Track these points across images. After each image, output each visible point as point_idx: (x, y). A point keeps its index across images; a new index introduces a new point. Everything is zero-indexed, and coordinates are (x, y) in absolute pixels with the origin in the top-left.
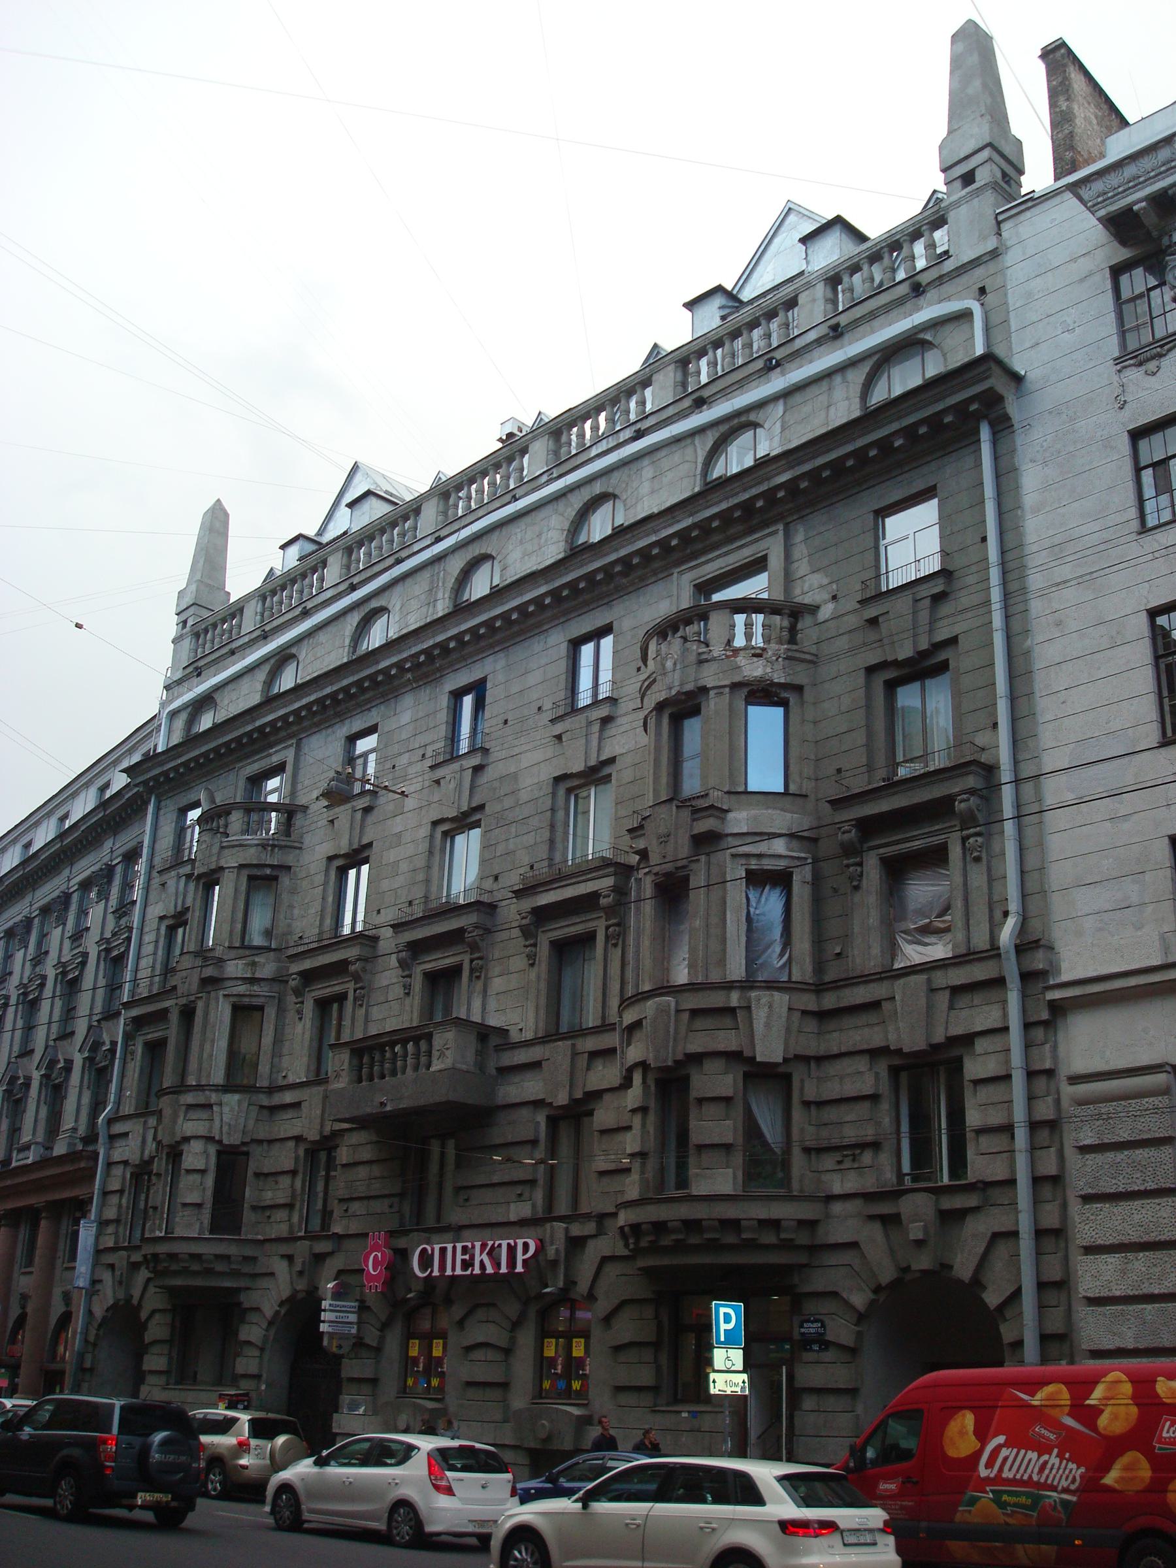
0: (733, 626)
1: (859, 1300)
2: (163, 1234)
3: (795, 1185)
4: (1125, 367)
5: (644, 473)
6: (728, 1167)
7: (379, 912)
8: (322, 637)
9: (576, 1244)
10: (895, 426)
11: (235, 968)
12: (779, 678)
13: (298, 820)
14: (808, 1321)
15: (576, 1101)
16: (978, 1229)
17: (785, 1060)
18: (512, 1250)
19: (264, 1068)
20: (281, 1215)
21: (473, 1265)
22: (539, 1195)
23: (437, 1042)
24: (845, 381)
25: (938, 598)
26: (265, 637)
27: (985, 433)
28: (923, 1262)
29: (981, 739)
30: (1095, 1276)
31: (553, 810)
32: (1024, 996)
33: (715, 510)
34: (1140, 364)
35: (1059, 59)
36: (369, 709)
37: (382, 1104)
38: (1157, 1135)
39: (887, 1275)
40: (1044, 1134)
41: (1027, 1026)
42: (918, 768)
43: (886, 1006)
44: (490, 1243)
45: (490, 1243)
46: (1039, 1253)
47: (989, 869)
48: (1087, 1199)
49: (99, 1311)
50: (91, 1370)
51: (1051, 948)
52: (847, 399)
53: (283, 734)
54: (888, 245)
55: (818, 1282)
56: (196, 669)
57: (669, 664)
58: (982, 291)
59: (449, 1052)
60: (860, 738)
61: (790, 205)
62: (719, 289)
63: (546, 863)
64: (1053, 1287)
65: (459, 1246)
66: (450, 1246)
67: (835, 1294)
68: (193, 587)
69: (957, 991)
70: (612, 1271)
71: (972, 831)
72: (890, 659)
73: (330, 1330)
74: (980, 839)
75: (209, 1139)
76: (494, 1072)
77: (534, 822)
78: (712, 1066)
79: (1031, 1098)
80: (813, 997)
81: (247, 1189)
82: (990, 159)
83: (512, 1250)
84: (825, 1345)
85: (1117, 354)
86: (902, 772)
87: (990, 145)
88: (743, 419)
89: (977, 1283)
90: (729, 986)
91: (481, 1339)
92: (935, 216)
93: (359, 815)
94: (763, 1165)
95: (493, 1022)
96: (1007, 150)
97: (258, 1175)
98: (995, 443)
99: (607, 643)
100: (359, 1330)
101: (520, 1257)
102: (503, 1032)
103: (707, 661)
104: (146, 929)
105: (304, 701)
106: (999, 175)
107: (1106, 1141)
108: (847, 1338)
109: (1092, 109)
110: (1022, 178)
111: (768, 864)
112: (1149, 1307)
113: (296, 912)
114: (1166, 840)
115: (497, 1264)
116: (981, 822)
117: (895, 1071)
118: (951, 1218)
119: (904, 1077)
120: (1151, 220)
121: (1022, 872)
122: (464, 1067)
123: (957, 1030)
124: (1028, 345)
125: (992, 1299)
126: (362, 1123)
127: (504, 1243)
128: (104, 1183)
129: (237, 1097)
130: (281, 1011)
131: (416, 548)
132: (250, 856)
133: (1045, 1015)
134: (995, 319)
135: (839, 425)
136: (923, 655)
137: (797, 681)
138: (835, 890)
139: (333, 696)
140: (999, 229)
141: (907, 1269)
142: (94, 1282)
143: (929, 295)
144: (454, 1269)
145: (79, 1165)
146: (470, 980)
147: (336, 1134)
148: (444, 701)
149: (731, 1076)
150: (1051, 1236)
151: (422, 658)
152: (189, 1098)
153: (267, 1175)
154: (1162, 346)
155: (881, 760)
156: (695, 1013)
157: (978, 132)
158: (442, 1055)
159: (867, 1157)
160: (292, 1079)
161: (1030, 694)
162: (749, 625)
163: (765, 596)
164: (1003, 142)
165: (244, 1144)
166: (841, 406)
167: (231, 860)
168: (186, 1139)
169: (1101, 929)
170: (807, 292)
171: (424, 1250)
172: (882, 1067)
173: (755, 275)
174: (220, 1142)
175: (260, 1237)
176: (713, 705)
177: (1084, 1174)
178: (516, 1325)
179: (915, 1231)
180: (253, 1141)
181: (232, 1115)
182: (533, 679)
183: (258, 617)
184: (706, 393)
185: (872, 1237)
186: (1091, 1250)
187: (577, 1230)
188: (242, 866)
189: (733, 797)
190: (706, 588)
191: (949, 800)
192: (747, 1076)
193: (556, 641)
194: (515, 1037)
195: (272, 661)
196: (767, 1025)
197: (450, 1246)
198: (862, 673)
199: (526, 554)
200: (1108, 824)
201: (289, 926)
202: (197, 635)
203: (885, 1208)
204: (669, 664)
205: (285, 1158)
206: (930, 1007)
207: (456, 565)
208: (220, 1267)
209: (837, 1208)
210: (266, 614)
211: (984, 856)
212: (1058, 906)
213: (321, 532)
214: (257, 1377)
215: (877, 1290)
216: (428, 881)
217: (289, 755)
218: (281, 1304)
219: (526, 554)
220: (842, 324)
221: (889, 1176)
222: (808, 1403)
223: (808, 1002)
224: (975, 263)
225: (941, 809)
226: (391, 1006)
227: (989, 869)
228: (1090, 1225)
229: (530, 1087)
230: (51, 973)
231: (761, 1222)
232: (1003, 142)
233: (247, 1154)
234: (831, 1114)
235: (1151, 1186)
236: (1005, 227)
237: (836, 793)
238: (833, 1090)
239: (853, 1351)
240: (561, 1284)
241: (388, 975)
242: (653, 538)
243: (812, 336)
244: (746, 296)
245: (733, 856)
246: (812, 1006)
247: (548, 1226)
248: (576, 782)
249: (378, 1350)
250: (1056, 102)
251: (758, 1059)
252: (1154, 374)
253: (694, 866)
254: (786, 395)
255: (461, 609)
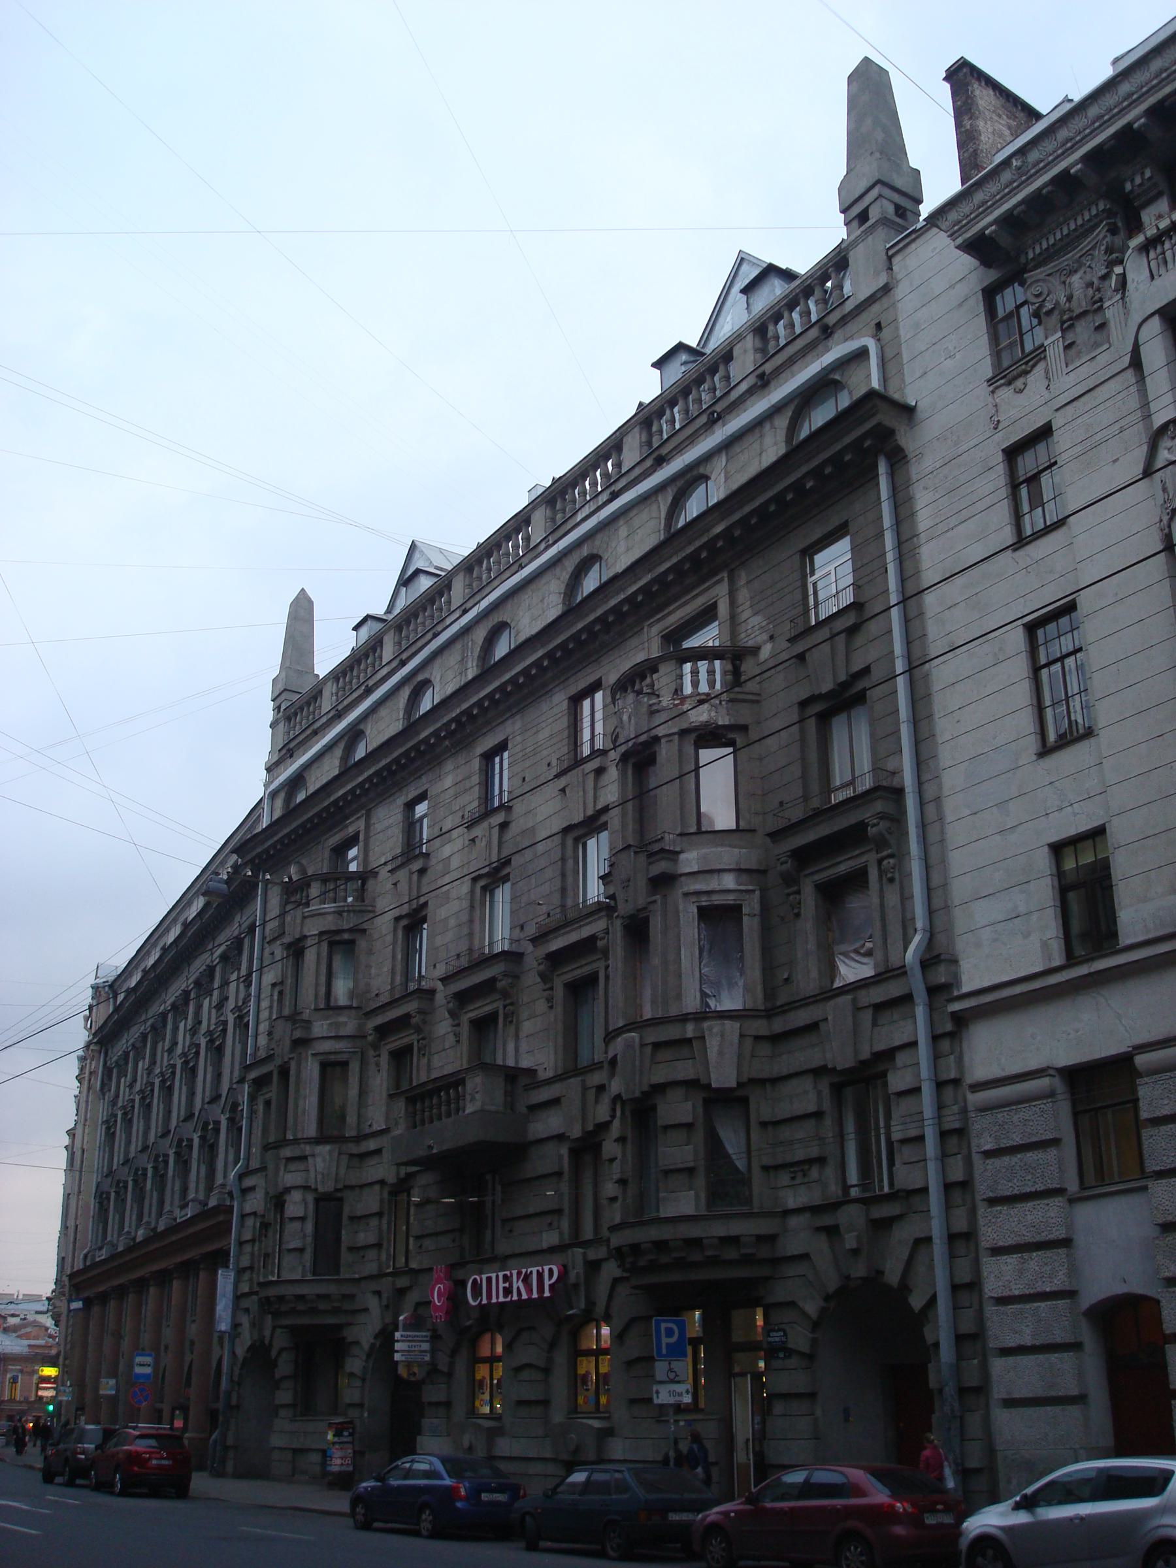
0: (681, 676)
1: (812, 1308)
2: (275, 1278)
3: (756, 1202)
4: (997, 388)
5: (621, 530)
6: (691, 1189)
7: (435, 966)
8: (383, 712)
9: (593, 1266)
10: (804, 469)
11: (320, 1028)
12: (724, 720)
13: (370, 884)
14: (774, 1331)
15: (589, 1133)
16: (904, 1234)
17: (740, 1085)
18: (540, 1275)
19: (351, 1119)
20: (372, 1254)
21: (511, 1292)
22: (565, 1224)
23: (469, 1085)
24: (773, 427)
25: (852, 631)
26: (339, 715)
27: (882, 468)
28: (859, 1270)
29: (891, 765)
30: (1001, 1276)
31: (563, 859)
32: (931, 1008)
33: (667, 565)
34: (1009, 383)
35: (963, 76)
36: (420, 777)
37: (430, 1147)
38: (1044, 1138)
39: (833, 1285)
40: (953, 1141)
41: (935, 1038)
42: (849, 793)
43: (822, 1026)
44: (524, 1271)
45: (524, 1271)
46: (952, 1256)
47: (902, 888)
48: (993, 1202)
49: (240, 1352)
50: (238, 1407)
51: (955, 962)
52: (775, 444)
53: (354, 806)
54: (802, 291)
55: (780, 1293)
56: (289, 750)
57: (625, 718)
58: (879, 326)
59: (479, 1095)
60: (796, 771)
61: (742, 255)
62: (681, 347)
63: (558, 910)
64: (967, 1289)
65: (501, 1274)
66: (494, 1276)
67: (792, 1304)
68: (284, 674)
69: (879, 1008)
70: (623, 1290)
71: (885, 853)
72: (816, 693)
73: (403, 1358)
74: (892, 861)
75: (306, 1188)
76: (524, 1110)
77: (549, 873)
78: (675, 1094)
79: (940, 1106)
80: (764, 1022)
81: (343, 1232)
82: (880, 196)
83: (540, 1275)
84: (790, 1353)
85: (990, 375)
86: (837, 798)
87: (879, 182)
88: (695, 473)
89: (905, 1287)
90: (684, 1018)
91: (525, 1361)
92: (838, 261)
93: (415, 877)
94: (725, 1185)
95: (525, 1063)
96: (899, 183)
97: (352, 1219)
98: (892, 475)
99: (599, 696)
100: (432, 1357)
101: (547, 1283)
102: (531, 1072)
103: (658, 711)
104: (263, 996)
105: (366, 775)
106: (891, 209)
107: (1002, 1146)
108: (803, 1345)
109: (1005, 120)
110: (921, 207)
111: (717, 900)
112: (1043, 1305)
113: (373, 971)
114: (1046, 849)
115: (529, 1290)
116: (890, 842)
117: (837, 1089)
118: (882, 1226)
119: (848, 1092)
120: (1005, 241)
121: (929, 889)
122: (493, 1108)
123: (880, 1047)
124: (918, 374)
125: (917, 1302)
126: (428, 1163)
127: (534, 1270)
128: (239, 1233)
129: (328, 1148)
130: (363, 1063)
131: (448, 621)
132: (329, 923)
133: (949, 1027)
134: (889, 353)
135: (762, 473)
136: (844, 686)
137: (742, 722)
138: (782, 918)
139: (387, 767)
140: (891, 263)
141: (848, 1278)
142: (236, 1326)
143: (836, 336)
144: (497, 1297)
145: (215, 1221)
146: (505, 1025)
147: (410, 1176)
148: (476, 764)
149: (689, 1104)
150: (962, 1239)
151: (453, 726)
152: (287, 1152)
153: (360, 1218)
154: (1026, 363)
155: (815, 788)
156: (657, 1046)
157: (870, 171)
158: (473, 1099)
159: (814, 1173)
160: (376, 1127)
161: (930, 716)
162: (695, 672)
163: (717, 644)
164: (895, 176)
165: (337, 1190)
166: (770, 448)
167: (313, 928)
168: (288, 1190)
169: (995, 940)
170: (739, 345)
171: (475, 1281)
172: (824, 1085)
173: (718, 327)
174: (708, 1086)
175: (357, 1276)
176: (666, 752)
177: (990, 1177)
178: (552, 1346)
179: (850, 1241)
180: (346, 1187)
181: (323, 1163)
182: (544, 734)
183: (334, 698)
184: (664, 451)
185: (820, 1247)
186: (997, 1251)
187: (593, 1255)
188: (321, 933)
189: (685, 838)
190: (674, 637)
191: (862, 826)
192: (707, 1102)
193: (559, 701)
194: (542, 1075)
195: (346, 738)
196: (721, 1053)
197: (494, 1276)
198: (796, 709)
199: (534, 619)
200: (998, 837)
201: (368, 985)
202: (288, 719)
203: (826, 1220)
204: (625, 718)
205: (371, 1201)
206: (856, 1025)
207: (480, 634)
208: (322, 1306)
209: (794, 1222)
210: (340, 693)
211: (897, 876)
212: (961, 922)
213: (388, 611)
214: (361, 1405)
215: (827, 1298)
216: (471, 935)
217: (361, 825)
218: (376, 1337)
219: (534, 619)
220: (767, 372)
221: (834, 1190)
222: (778, 1408)
223: (760, 1027)
224: (871, 300)
225: (855, 836)
226: (446, 1052)
227: (902, 888)
228: (997, 1227)
229: (550, 1123)
230: (203, 1042)
231: (722, 1240)
232: (895, 176)
233: (341, 1200)
234: (786, 1133)
235: (1040, 1187)
236: (895, 261)
237: (773, 825)
238: (785, 1110)
239: (810, 1357)
240: (583, 1306)
241: (443, 1027)
242: (622, 596)
243: (744, 387)
244: (708, 351)
245: (686, 895)
246: (764, 1031)
247: (570, 1252)
248: (581, 832)
249: (450, 1375)
250: (961, 122)
251: (714, 1086)
252: (1021, 391)
253: (652, 907)
254: (727, 445)
255: (487, 672)
